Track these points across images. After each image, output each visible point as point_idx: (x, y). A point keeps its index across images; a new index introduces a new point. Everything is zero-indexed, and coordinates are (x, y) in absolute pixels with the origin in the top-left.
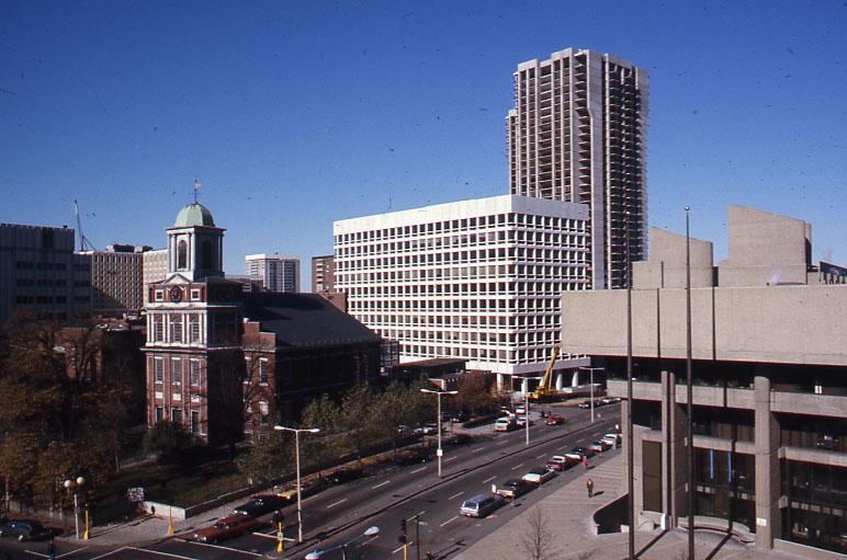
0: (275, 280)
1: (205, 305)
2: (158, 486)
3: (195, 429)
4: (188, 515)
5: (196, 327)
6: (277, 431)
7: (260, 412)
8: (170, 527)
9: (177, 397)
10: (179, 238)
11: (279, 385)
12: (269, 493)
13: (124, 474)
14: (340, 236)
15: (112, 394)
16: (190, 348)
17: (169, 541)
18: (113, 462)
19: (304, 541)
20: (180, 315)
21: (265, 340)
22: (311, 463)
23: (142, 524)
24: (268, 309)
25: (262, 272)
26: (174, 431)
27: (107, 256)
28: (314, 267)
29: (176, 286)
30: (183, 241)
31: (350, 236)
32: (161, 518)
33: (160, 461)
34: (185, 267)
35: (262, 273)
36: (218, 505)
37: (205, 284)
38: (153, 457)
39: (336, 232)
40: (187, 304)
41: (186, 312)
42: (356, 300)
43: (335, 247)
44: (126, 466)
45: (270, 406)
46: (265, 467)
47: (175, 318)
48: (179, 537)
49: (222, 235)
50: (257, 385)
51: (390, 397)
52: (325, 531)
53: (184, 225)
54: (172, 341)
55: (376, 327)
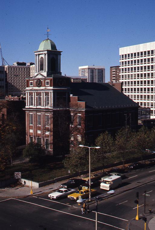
0: (93, 79)
1: (52, 88)
2: (28, 172)
3: (47, 147)
4: (40, 186)
5: (48, 99)
6: (81, 147)
7: (77, 140)
8: (31, 191)
9: (39, 132)
10: (40, 56)
11: (87, 127)
12: (79, 178)
13: (14, 166)
14: (123, 55)
15: (7, 129)
16: (46, 109)
17: (28, 197)
18: (10, 161)
19: (91, 201)
20: (41, 93)
21: (80, 105)
22: (95, 166)
23: (19, 189)
24: (82, 90)
25: (87, 75)
26: (37, 147)
27: (14, 67)
28: (111, 72)
29: (39, 79)
30: (42, 58)
31: (130, 55)
32: (28, 187)
33: (30, 161)
34: (43, 70)
35: (87, 75)
36: (54, 182)
37: (52, 78)
38: (28, 159)
39: (121, 54)
40: (43, 88)
41: (43, 91)
42: (127, 87)
43: (120, 61)
44: (15, 163)
45: (82, 137)
46: (76, 166)
47: (39, 94)
48: (35, 195)
49: (60, 55)
50: (76, 126)
51: (141, 135)
52: (102, 197)
53: (42, 50)
54: (37, 106)
55: (136, 101)
